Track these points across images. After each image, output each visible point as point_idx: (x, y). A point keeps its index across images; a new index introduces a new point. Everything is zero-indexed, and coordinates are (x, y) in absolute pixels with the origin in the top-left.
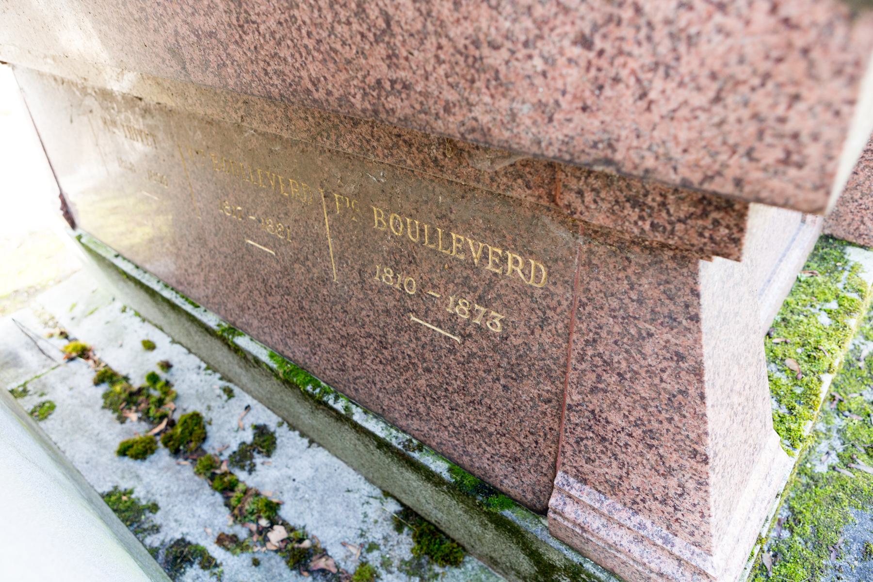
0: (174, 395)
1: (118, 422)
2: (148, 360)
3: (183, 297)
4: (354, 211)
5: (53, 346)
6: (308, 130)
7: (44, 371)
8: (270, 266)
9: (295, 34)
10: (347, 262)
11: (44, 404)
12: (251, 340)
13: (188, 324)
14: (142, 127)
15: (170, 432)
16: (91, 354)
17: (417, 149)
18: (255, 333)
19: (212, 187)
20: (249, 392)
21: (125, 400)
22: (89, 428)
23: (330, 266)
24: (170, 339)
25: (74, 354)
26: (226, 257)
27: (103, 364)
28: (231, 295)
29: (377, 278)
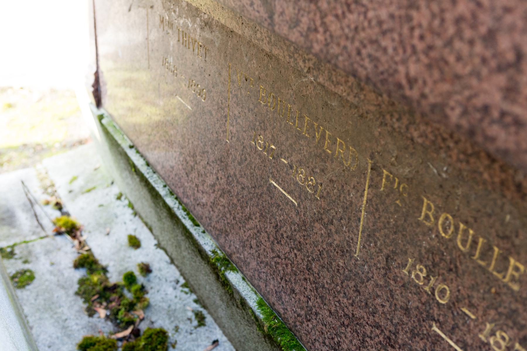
0: (146, 303)
1: (86, 313)
2: (130, 257)
3: (185, 210)
4: (401, 194)
5: (47, 215)
6: (379, 105)
7: (34, 237)
8: (288, 215)
9: (405, 31)
10: (376, 243)
11: (25, 271)
12: (243, 279)
13: (181, 238)
14: (197, 37)
15: (133, 341)
16: (78, 233)
17: (501, 167)
18: (249, 273)
19: (251, 117)
20: (222, 326)
21: (98, 293)
22: (59, 311)
23: (355, 241)
24: (155, 242)
25: (63, 229)
26: (243, 188)
27: (86, 248)
28: (236, 227)
29: (405, 271)
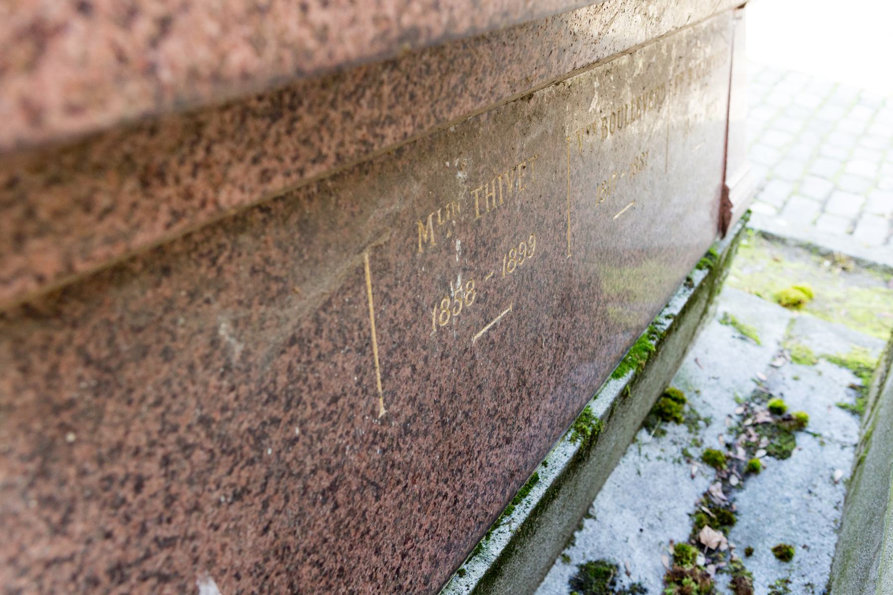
12: (595, 398)
